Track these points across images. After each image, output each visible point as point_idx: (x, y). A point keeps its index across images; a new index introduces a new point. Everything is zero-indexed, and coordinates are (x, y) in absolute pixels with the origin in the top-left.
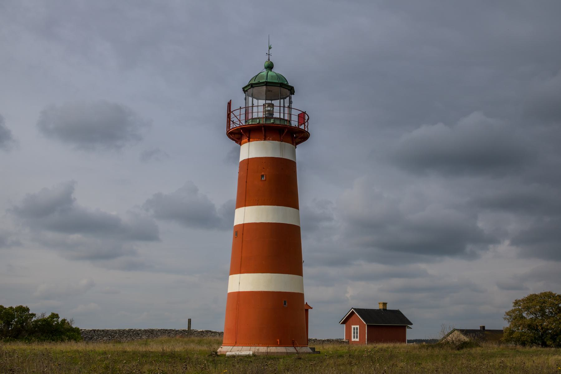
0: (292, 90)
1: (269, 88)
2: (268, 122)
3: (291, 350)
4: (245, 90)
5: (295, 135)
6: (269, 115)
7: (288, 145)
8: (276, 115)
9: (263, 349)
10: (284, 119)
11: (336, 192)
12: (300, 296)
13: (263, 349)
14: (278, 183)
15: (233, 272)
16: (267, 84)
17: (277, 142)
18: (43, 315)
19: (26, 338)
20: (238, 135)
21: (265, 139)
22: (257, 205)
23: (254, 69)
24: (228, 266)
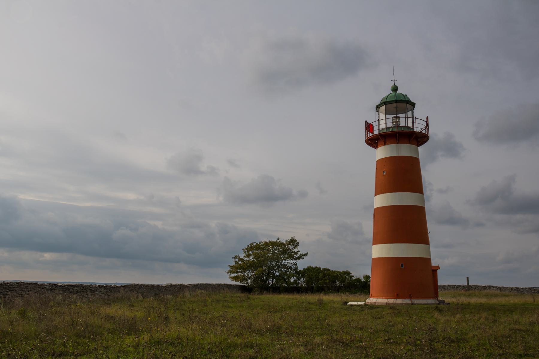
0: (413, 105)
1: (388, 106)
2: (388, 131)
3: (408, 301)
4: (378, 107)
5: (421, 139)
6: (397, 125)
7: (413, 146)
8: (403, 124)
9: (391, 301)
10: (408, 127)
11: (443, 180)
12: (428, 261)
13: (391, 301)
14: (402, 175)
15: (373, 244)
16: (396, 101)
17: (394, 145)
18: (360, 295)
19: (303, 303)
20: (374, 141)
21: (385, 144)
22: (381, 193)
23: (386, 92)
24: (427, 245)
